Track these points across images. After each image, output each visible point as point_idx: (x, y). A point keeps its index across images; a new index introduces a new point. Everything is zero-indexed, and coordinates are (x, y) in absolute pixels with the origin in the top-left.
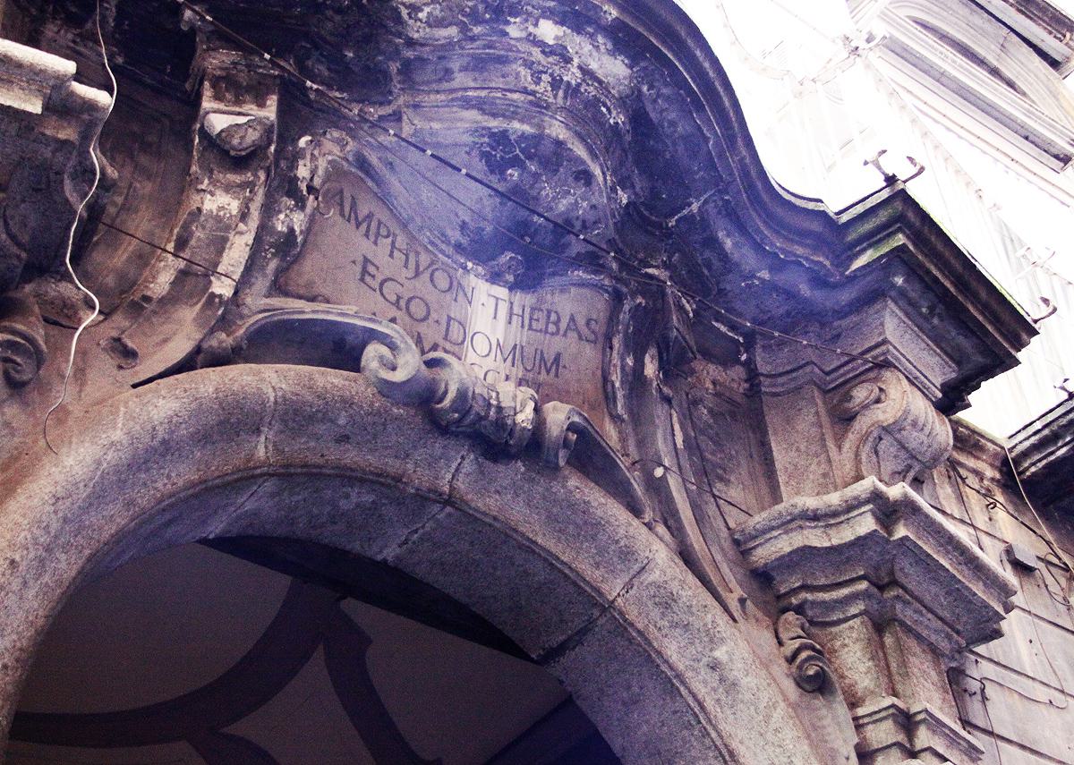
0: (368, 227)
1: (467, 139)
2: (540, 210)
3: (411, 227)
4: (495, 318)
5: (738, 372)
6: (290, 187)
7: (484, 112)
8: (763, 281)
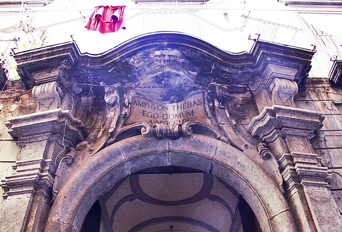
1: (151, 80)
2: (173, 86)
3: (152, 101)
4: (174, 110)
5: (248, 93)
6: (124, 105)
7: (152, 74)
8: (240, 73)
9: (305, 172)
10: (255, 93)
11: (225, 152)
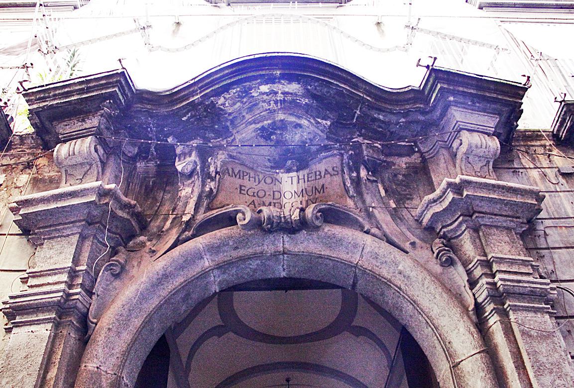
0: (240, 176)
1: (254, 134)
2: (290, 143)
3: (254, 168)
4: (292, 184)
5: (417, 155)
7: (255, 123)
8: (403, 122)
9: (512, 287)
10: (428, 155)
11: (378, 255)
